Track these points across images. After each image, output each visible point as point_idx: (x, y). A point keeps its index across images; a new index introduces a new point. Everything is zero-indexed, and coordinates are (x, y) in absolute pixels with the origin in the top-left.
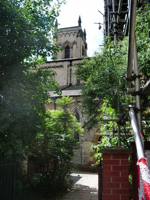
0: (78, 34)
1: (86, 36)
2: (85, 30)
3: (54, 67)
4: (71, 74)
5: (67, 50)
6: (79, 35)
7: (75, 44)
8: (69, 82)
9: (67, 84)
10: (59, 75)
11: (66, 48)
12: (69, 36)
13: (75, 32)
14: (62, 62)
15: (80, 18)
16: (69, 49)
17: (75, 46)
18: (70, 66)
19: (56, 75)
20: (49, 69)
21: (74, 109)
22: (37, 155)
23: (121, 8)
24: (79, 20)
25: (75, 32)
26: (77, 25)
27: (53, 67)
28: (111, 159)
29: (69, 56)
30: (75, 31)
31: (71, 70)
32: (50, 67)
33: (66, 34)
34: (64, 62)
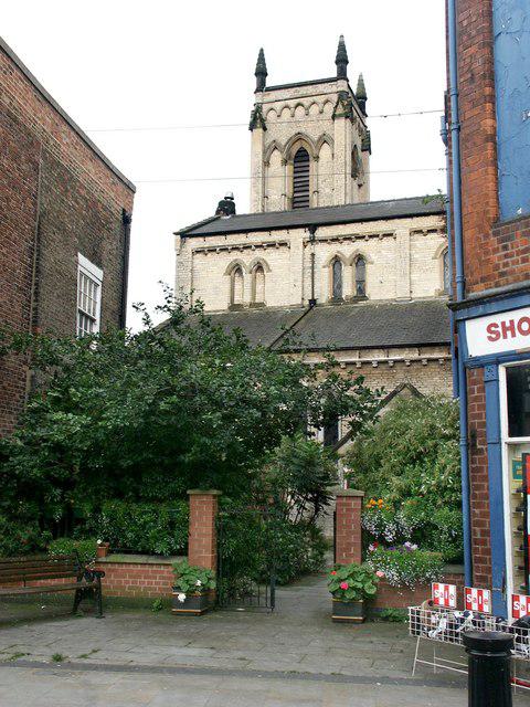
2: (361, 84)
3: (261, 246)
4: (313, 268)
5: (299, 164)
6: (340, 110)
10: (276, 271)
14: (285, 231)
15: (342, 48)
17: (325, 152)
18: (310, 244)
19: (270, 270)
20: (295, 356)
22: (101, 427)
23: (491, 423)
25: (327, 101)
33: (299, 105)
34: (291, 231)
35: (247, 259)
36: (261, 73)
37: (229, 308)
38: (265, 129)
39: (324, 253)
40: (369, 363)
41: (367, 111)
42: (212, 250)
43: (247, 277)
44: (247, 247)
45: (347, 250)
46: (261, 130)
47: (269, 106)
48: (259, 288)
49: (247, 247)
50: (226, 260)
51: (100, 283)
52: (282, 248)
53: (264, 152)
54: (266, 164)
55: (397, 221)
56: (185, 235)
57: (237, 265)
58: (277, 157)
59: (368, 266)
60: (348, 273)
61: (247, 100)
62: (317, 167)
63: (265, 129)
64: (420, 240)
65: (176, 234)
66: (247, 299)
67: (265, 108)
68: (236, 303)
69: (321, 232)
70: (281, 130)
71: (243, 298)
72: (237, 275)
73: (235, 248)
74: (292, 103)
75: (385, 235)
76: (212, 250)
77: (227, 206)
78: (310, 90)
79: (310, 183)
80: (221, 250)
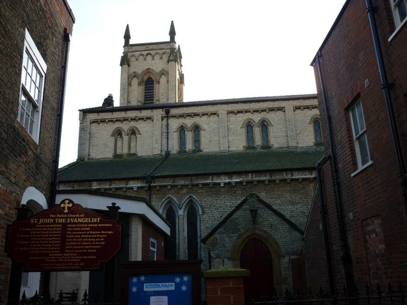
0: (169, 57)
1: (182, 60)
7: (163, 76)
8: (165, 148)
9: (161, 151)
11: (147, 81)
12: (153, 59)
13: (164, 53)
14: (150, 111)
16: (153, 84)
21: (187, 199)
24: (170, 31)
25: (164, 53)
26: (168, 39)
27: (132, 119)
28: (231, 285)
29: (153, 97)
30: (163, 51)
31: (168, 125)
32: (127, 120)
33: (148, 54)
35: (125, 127)
36: (127, 37)
37: (114, 156)
38: (129, 66)
39: (174, 124)
40: (219, 184)
42: (103, 121)
44: (125, 120)
45: (189, 122)
48: (133, 145)
49: (125, 120)
50: (112, 127)
51: (44, 75)
52: (149, 121)
53: (128, 78)
54: (130, 84)
55: (219, 106)
57: (119, 130)
58: (135, 82)
59: (202, 132)
60: (189, 136)
63: (129, 66)
64: (233, 117)
65: (80, 110)
66: (125, 151)
67: (129, 54)
68: (118, 153)
69: (174, 111)
70: (139, 66)
71: (123, 150)
73: (118, 120)
75: (212, 114)
76: (103, 121)
77: (109, 101)
78: (155, 47)
80: (109, 121)
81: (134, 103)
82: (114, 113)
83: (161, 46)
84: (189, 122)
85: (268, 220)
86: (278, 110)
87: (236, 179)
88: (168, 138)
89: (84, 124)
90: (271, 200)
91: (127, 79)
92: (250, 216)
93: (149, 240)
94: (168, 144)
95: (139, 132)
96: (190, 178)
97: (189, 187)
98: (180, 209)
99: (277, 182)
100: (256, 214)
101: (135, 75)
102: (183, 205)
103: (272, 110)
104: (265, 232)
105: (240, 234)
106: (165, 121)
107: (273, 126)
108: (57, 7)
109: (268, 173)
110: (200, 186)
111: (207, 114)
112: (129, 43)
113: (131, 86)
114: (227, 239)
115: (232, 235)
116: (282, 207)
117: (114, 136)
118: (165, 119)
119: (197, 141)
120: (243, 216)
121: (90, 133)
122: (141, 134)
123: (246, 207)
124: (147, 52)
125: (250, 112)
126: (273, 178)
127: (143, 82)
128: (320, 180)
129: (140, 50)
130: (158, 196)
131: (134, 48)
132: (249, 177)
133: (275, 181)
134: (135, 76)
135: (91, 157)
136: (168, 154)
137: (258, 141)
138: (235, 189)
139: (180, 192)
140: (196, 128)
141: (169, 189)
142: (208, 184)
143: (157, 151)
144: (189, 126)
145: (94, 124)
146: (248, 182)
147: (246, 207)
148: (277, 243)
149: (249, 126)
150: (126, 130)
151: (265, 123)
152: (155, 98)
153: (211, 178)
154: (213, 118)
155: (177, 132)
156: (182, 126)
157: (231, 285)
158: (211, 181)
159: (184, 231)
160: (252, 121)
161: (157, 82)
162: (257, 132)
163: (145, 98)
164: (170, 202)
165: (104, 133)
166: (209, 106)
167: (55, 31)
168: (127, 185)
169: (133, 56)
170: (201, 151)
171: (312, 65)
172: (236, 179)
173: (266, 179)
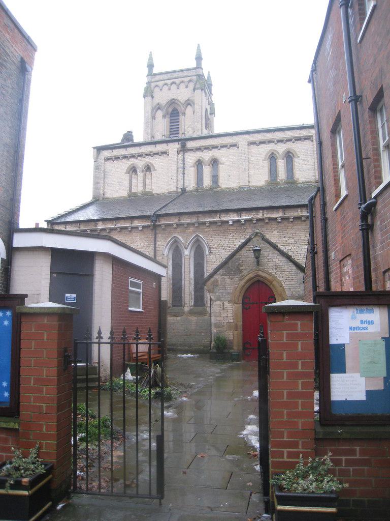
9: (177, 188)
11: (172, 113)
13: (190, 81)
16: (179, 116)
19: (155, 170)
25: (190, 81)
26: (193, 64)
28: (45, 321)
31: (184, 159)
35: (140, 163)
36: (150, 66)
38: (152, 97)
40: (227, 222)
41: (213, 92)
42: (117, 158)
43: (140, 175)
44: (140, 155)
45: (206, 156)
46: (150, 97)
47: (155, 84)
48: (148, 182)
49: (140, 155)
54: (154, 118)
56: (99, 149)
57: (134, 167)
58: (160, 114)
59: (220, 166)
61: (142, 81)
62: (184, 120)
63: (152, 97)
64: (254, 149)
65: (94, 148)
69: (190, 145)
70: (163, 97)
71: (138, 188)
72: (133, 174)
73: (132, 156)
74: (169, 82)
76: (117, 158)
77: (128, 137)
78: (180, 74)
79: (180, 123)
80: (124, 158)
81: (158, 137)
82: (128, 149)
83: (186, 73)
84: (206, 156)
85: (272, 261)
86: (305, 139)
87: (245, 217)
88: (184, 174)
89: (98, 162)
90: (284, 239)
91: (150, 111)
92: (253, 256)
93: (128, 280)
94: (184, 180)
95: (154, 168)
96: (196, 215)
97: (196, 225)
98: (186, 248)
99: (291, 219)
100: (259, 254)
101: (159, 107)
102: (189, 244)
103: (298, 139)
104: (270, 274)
105: (242, 276)
106: (181, 156)
107: (299, 157)
108: (7, 35)
109: (281, 210)
110: (207, 225)
111: (226, 146)
112: (152, 72)
113: (155, 119)
114: (228, 281)
115: (233, 276)
116: (295, 248)
117: (129, 173)
118: (181, 154)
119: (215, 178)
120: (248, 255)
121: (104, 171)
122: (156, 170)
123: (249, 247)
124: (172, 81)
125: (274, 142)
126: (287, 215)
127: (168, 114)
128: (312, 217)
129: (165, 78)
130: (164, 236)
131: (158, 78)
132: (260, 215)
133: (288, 219)
134: (159, 108)
135: (106, 196)
136: (184, 190)
137: (282, 175)
138: (245, 228)
139: (186, 231)
140: (214, 162)
141: (175, 228)
142: (215, 223)
143: (173, 188)
144: (207, 160)
145: (109, 162)
146: (259, 220)
147: (249, 247)
148: (281, 286)
149: (272, 158)
150: (141, 167)
151: (291, 154)
152: (181, 131)
153: (218, 216)
154: (233, 150)
155: (193, 167)
156: (199, 160)
157: (45, 321)
158: (218, 219)
159: (190, 271)
160: (275, 153)
161: (182, 113)
162: (281, 165)
163: (170, 132)
164: (176, 241)
165: (118, 172)
166: (228, 137)
167: (5, 61)
168: (132, 224)
169: (157, 86)
170: (219, 187)
171: (309, 82)
172: (245, 217)
173: (278, 216)
